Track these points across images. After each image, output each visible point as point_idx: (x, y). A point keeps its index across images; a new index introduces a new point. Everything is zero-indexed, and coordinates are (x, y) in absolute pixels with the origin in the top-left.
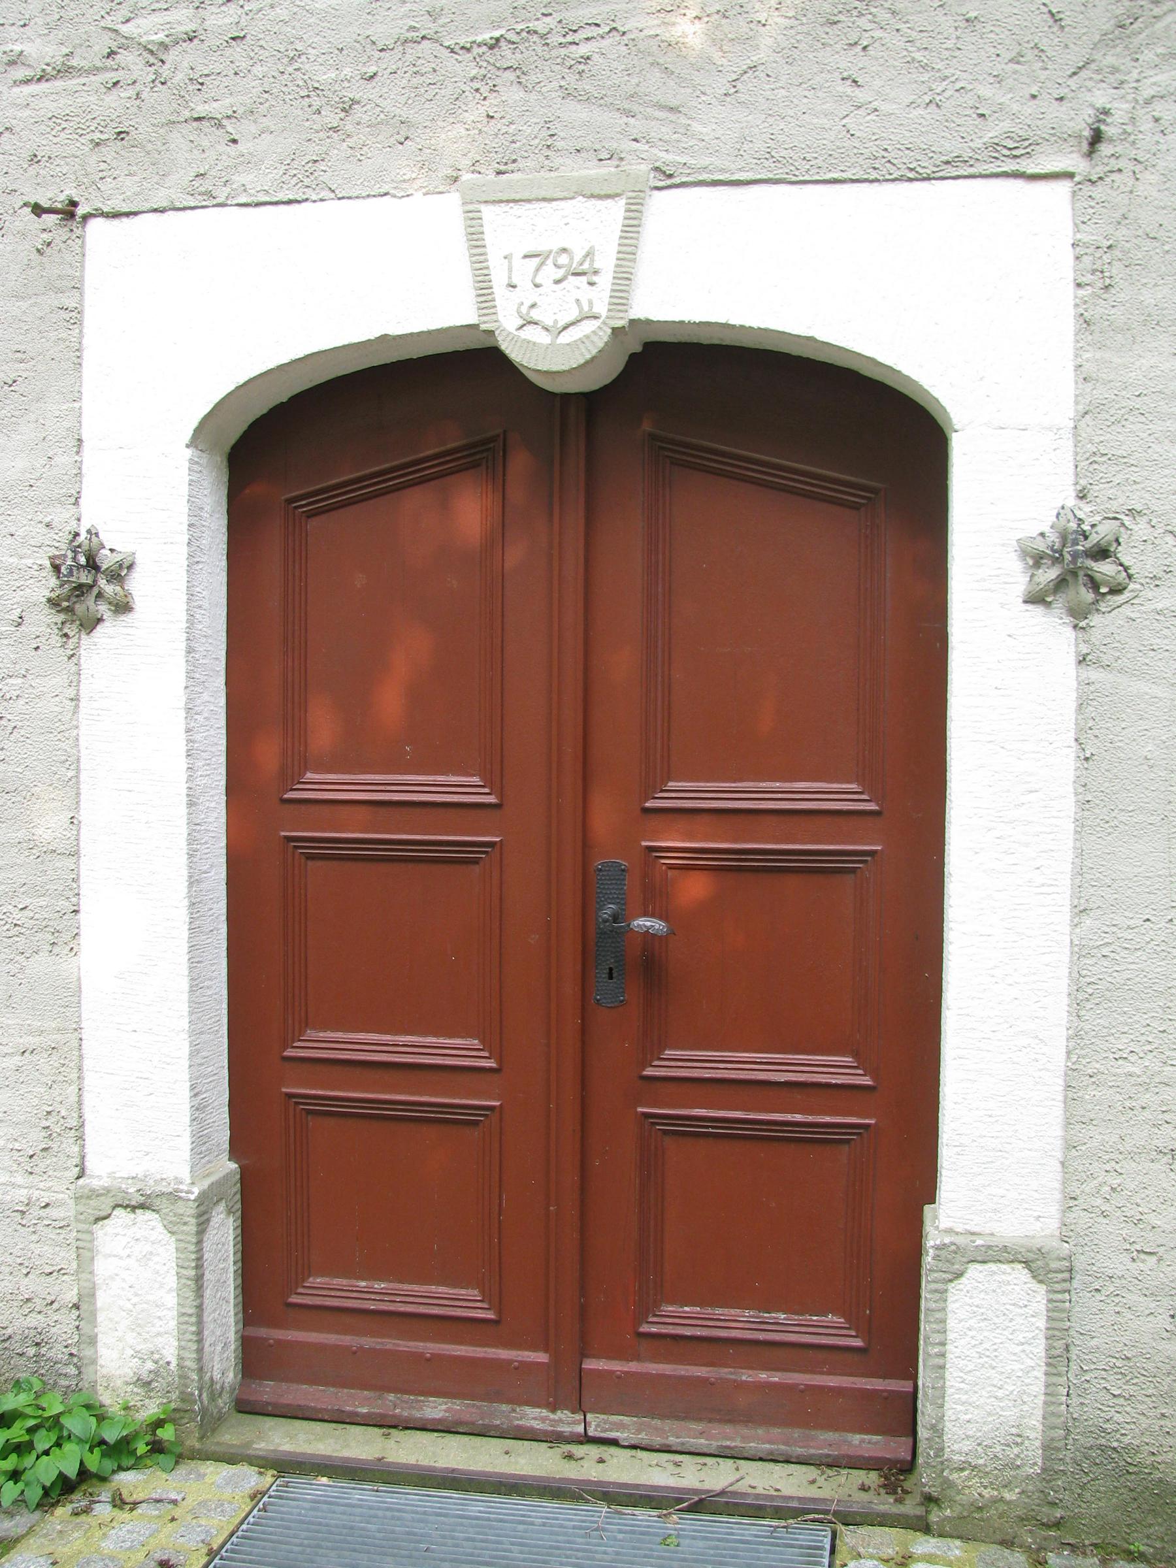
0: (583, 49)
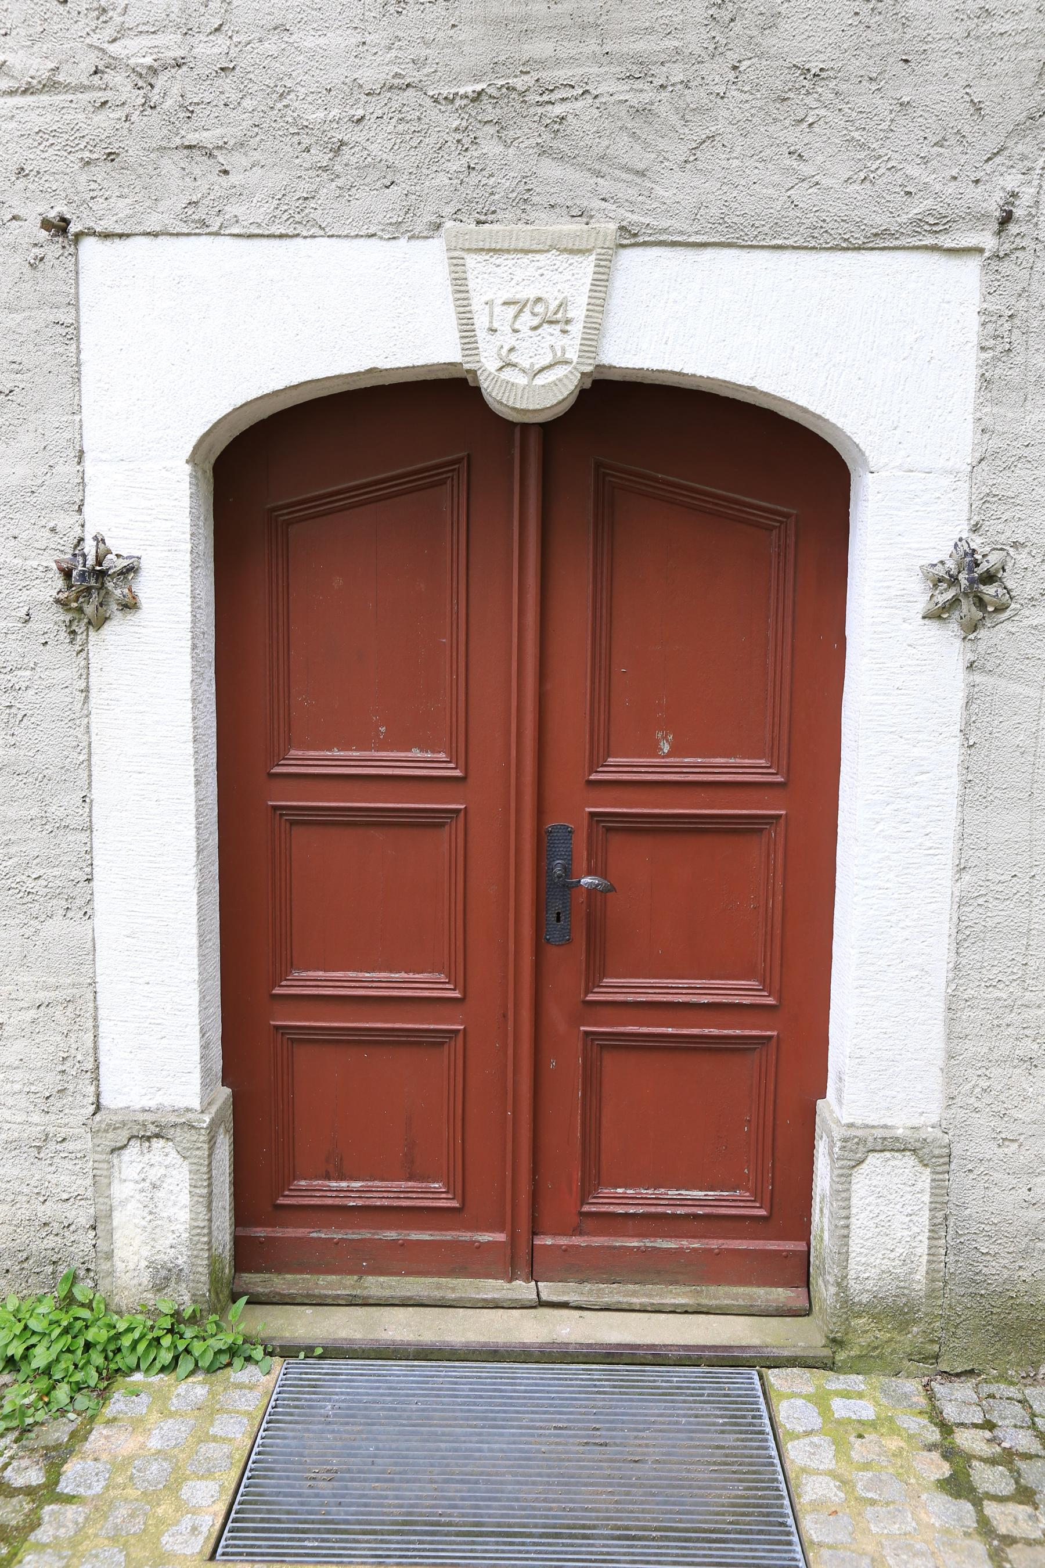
0: (558, 110)
